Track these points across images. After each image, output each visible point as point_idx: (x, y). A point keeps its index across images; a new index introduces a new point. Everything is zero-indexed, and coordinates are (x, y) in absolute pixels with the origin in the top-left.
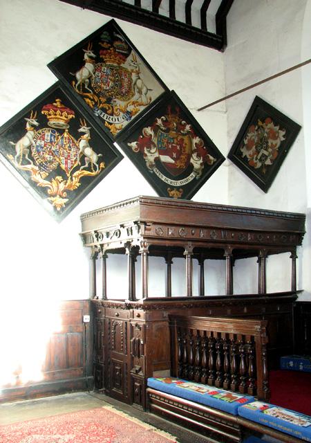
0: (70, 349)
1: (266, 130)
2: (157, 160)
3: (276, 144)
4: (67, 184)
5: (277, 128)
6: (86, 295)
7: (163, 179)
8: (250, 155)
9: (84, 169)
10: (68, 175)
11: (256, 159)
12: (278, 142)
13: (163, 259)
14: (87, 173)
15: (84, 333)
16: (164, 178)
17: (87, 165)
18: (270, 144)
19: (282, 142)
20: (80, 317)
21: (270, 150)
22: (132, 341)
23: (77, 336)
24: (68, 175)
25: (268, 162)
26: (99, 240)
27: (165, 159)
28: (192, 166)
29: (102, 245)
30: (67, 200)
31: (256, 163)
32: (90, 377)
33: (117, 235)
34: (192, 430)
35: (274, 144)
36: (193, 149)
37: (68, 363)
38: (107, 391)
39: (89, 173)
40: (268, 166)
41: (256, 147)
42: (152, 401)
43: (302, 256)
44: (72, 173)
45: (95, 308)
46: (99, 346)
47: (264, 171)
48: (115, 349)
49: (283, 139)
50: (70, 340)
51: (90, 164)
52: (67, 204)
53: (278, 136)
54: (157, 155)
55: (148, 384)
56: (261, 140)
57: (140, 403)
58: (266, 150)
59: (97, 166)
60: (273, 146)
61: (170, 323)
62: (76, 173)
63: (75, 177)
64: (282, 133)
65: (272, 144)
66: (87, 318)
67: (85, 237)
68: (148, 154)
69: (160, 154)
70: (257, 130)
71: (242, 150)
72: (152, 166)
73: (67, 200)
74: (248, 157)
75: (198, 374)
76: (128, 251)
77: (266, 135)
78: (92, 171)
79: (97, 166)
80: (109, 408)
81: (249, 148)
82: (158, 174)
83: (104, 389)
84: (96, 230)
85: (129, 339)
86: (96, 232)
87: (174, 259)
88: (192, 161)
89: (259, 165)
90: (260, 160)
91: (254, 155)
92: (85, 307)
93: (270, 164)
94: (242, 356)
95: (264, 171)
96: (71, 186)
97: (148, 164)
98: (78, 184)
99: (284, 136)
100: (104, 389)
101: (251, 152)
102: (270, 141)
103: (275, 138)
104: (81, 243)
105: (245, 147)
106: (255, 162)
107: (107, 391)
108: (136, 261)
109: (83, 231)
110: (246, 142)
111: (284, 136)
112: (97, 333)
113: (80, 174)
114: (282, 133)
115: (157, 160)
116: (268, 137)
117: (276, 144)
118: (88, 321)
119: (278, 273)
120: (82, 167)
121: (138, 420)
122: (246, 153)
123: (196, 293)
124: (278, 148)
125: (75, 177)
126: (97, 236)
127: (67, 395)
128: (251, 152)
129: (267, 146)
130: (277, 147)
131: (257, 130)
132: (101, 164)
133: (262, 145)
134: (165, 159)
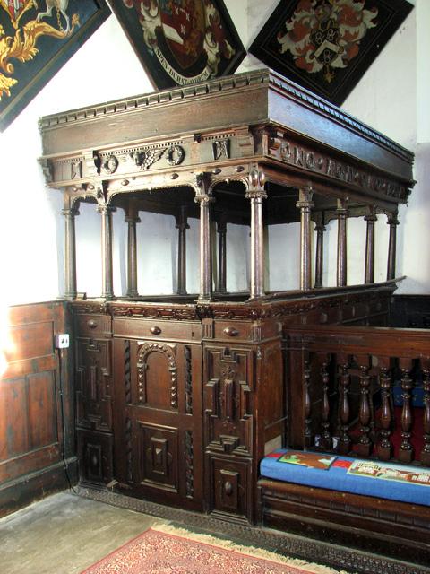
0: (35, 407)
1: (336, 8)
2: (159, 31)
3: (356, 35)
4: (14, 44)
5: (360, 6)
6: (53, 291)
7: (168, 71)
8: (298, 50)
9: (45, 19)
10: (16, 26)
11: (312, 56)
12: (361, 31)
13: (171, 219)
14: (50, 29)
15: (58, 371)
16: (168, 69)
17: (48, 12)
18: (342, 33)
19: (369, 31)
20: (49, 339)
21: (343, 43)
22: (210, 384)
23: (45, 379)
24: (16, 26)
25: (338, 63)
26: (103, 170)
27: (171, 33)
28: (204, 55)
29: (106, 184)
30: (15, 81)
31: (312, 65)
32: (71, 460)
33: (171, 158)
34: (278, 529)
35: (352, 32)
36: (207, 25)
37: (31, 436)
38: (122, 485)
39: (52, 29)
40: (338, 70)
41: (313, 37)
42: (269, 505)
43: (405, 221)
44: (23, 23)
45: (75, 313)
46: (93, 395)
47: (329, 78)
48: (146, 401)
49: (372, 25)
50: (33, 389)
51: (54, 10)
52: (14, 89)
53: (361, 20)
54: (158, 22)
55: (263, 472)
56: (324, 25)
57: (240, 510)
58: (334, 42)
59: (67, 18)
60: (348, 36)
61: (284, 344)
62: (30, 25)
63: (31, 33)
64: (370, 15)
65: (346, 32)
66: (64, 341)
67: (51, 168)
68: (147, 18)
69: (162, 22)
70: (315, 8)
71: (280, 41)
72: (152, 41)
73: (15, 81)
74: (293, 51)
75: (364, 441)
76: (101, 201)
77: (334, 16)
78: (58, 29)
79: (67, 18)
80: (163, 527)
81: (295, 36)
82: (160, 60)
83: (113, 483)
84: (96, 149)
85: (196, 383)
86: (96, 153)
87: (229, 226)
88: (205, 46)
89: (317, 67)
90: (321, 59)
91: (306, 49)
92: (58, 316)
93: (343, 66)
94: (385, 396)
95: (329, 78)
96: (20, 50)
97: (146, 37)
98: (34, 51)
99: (373, 21)
100: (113, 483)
101: (301, 44)
102: (343, 29)
103: (354, 21)
104: (37, 175)
105: (287, 36)
106: (309, 61)
107: (122, 485)
108: (188, 227)
109: (45, 154)
110: (290, 27)
111: (373, 21)
112: (87, 372)
113: (37, 29)
114: (370, 15)
115: (159, 31)
116: (339, 22)
117: (356, 35)
118: (66, 345)
119: (349, 252)
120: (40, 15)
121: (264, 551)
122: (286, 44)
123: (330, 281)
124: (361, 40)
125: (31, 33)
126: (98, 163)
127: (37, 506)
128: (301, 44)
129: (336, 36)
130: (358, 38)
131: (315, 8)
132: (74, 16)
133: (325, 33)
134: (171, 33)
